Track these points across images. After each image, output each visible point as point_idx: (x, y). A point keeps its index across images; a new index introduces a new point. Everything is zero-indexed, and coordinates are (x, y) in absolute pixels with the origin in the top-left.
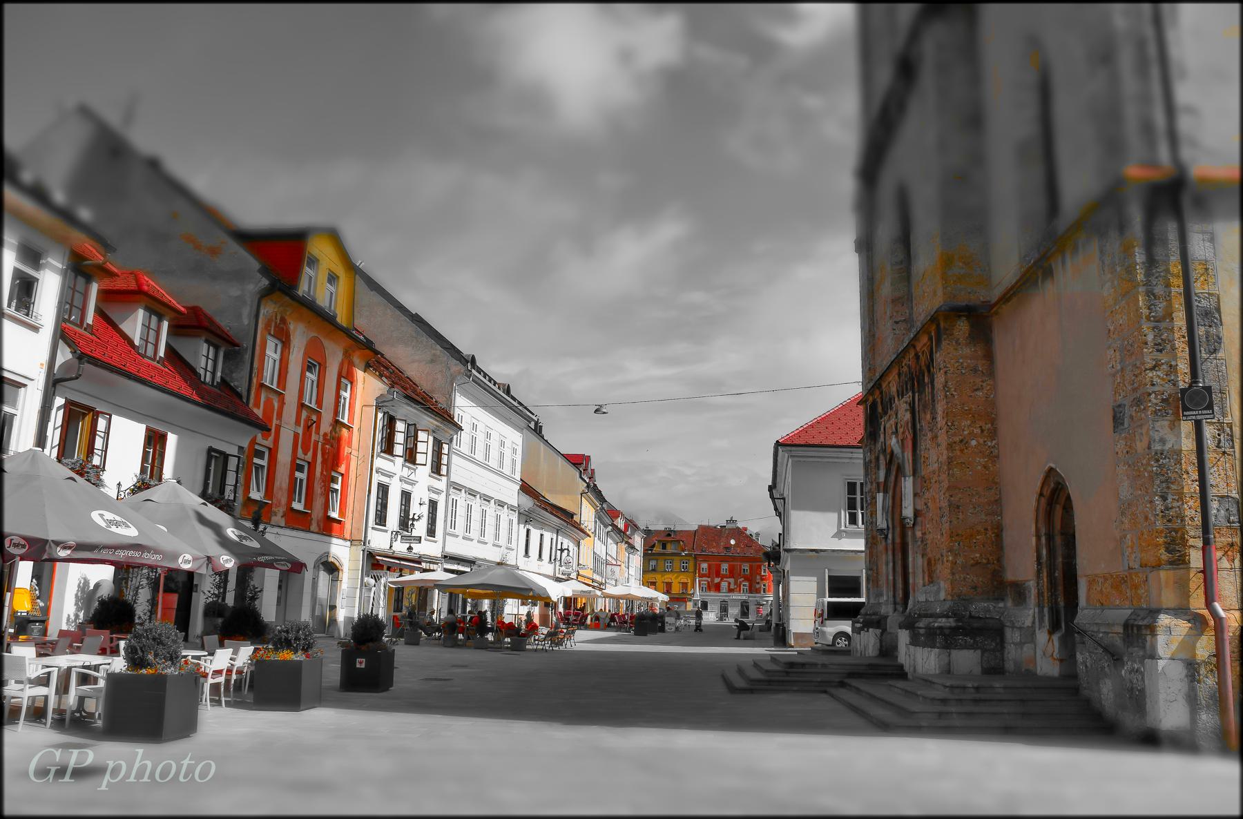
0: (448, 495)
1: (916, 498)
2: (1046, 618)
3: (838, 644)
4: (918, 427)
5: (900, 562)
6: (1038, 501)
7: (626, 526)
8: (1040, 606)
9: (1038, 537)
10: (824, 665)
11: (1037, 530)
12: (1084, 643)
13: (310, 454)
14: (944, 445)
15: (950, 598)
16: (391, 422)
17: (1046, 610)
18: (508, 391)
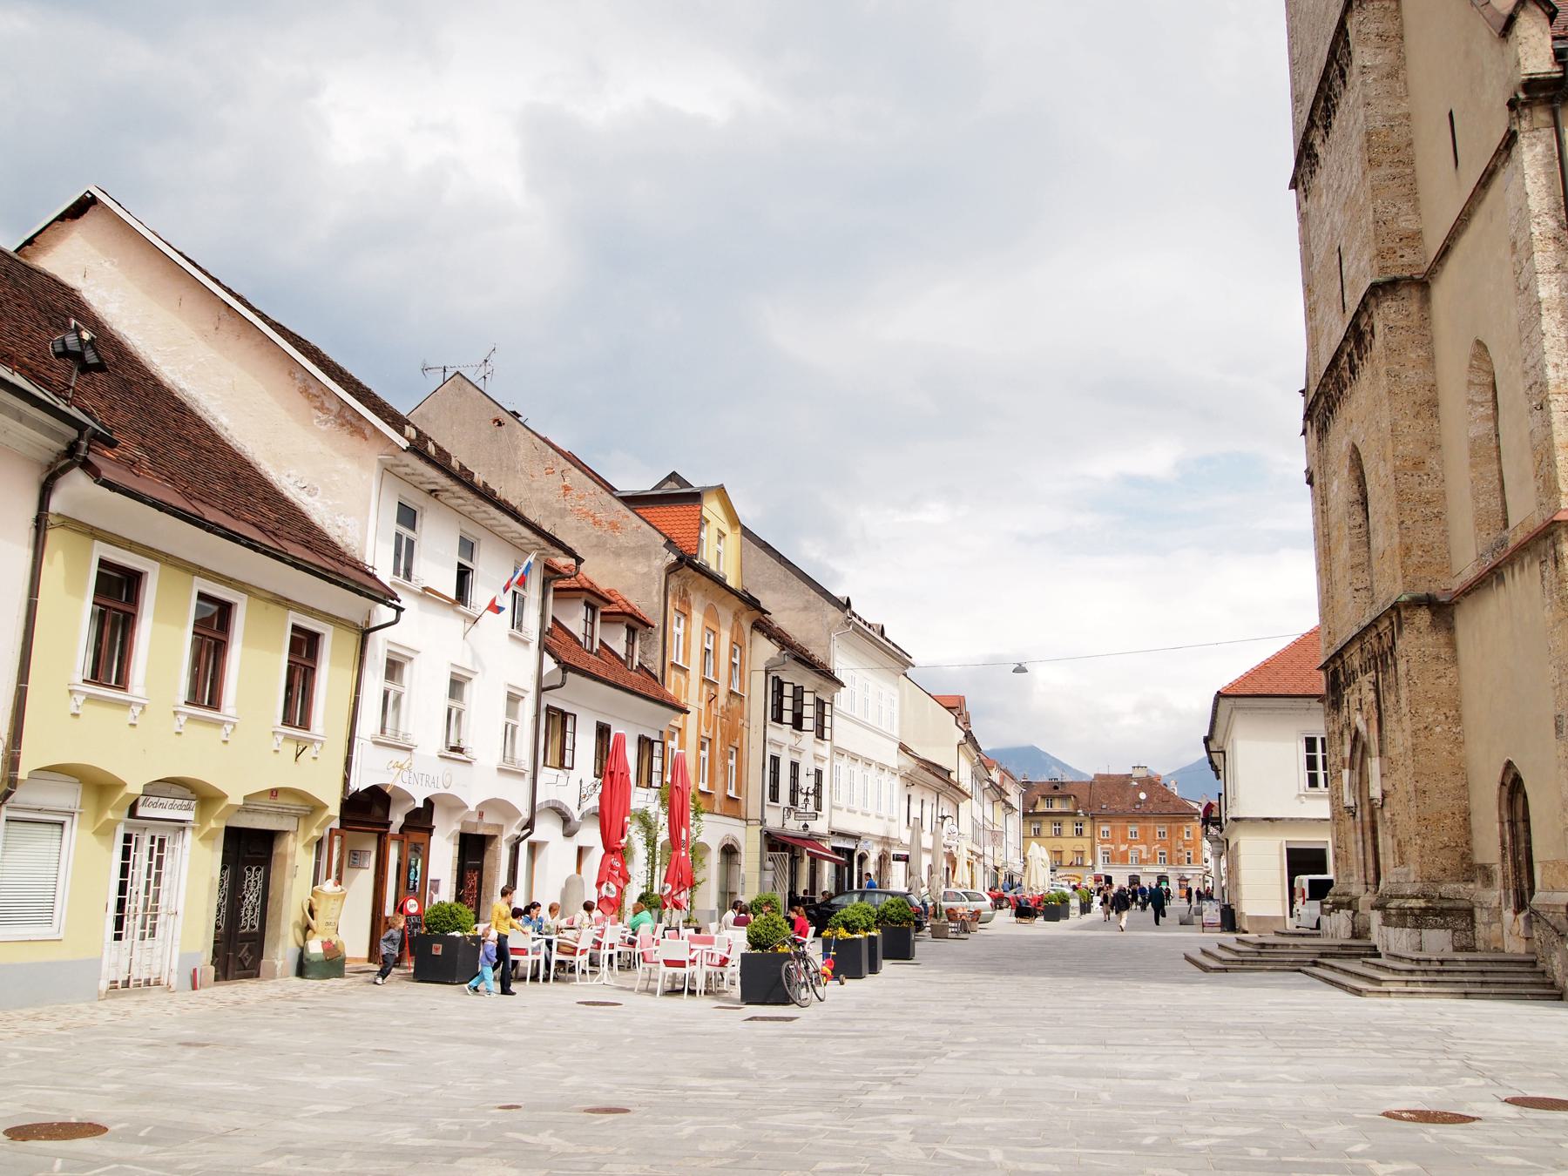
0: (832, 762)
1: (1384, 778)
2: (1512, 899)
3: (249, 869)
4: (1383, 707)
5: (1370, 841)
6: (1500, 789)
7: (1003, 778)
8: (1505, 887)
9: (1502, 823)
10: (1296, 946)
11: (1501, 816)
12: (1538, 922)
13: (711, 730)
14: (1408, 732)
15: (1419, 880)
16: (779, 685)
17: (1511, 892)
18: (882, 633)
